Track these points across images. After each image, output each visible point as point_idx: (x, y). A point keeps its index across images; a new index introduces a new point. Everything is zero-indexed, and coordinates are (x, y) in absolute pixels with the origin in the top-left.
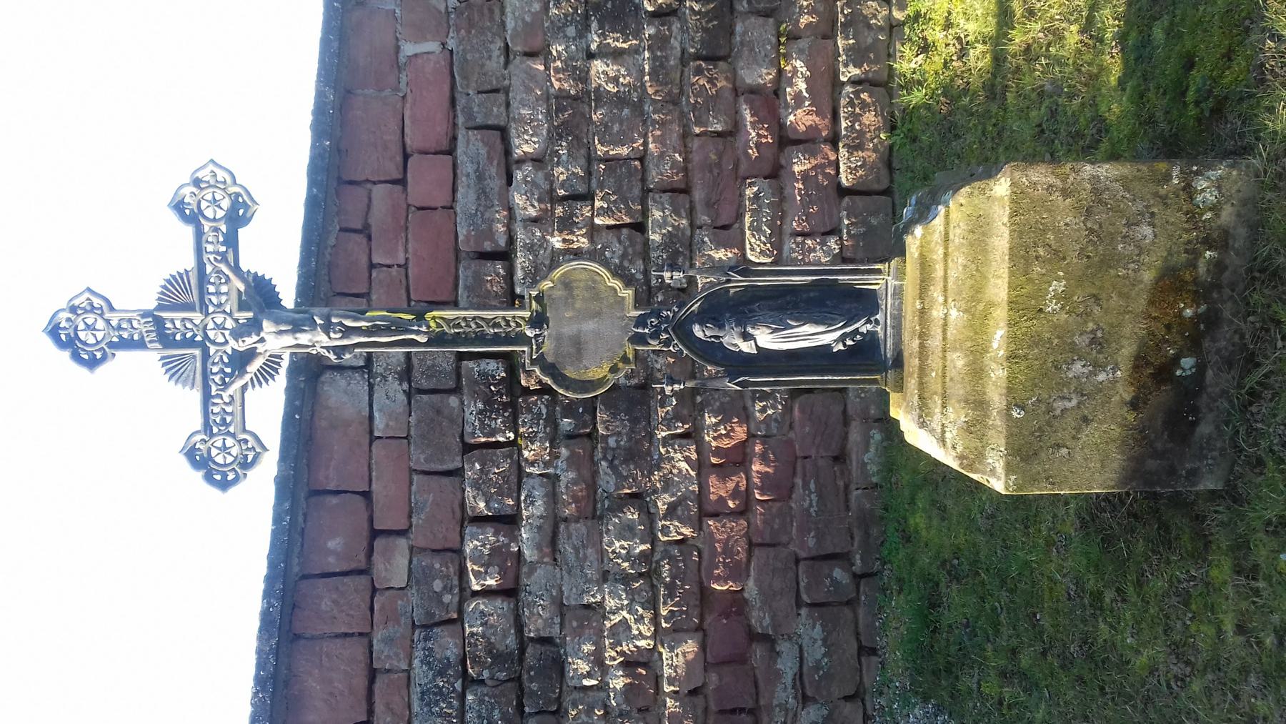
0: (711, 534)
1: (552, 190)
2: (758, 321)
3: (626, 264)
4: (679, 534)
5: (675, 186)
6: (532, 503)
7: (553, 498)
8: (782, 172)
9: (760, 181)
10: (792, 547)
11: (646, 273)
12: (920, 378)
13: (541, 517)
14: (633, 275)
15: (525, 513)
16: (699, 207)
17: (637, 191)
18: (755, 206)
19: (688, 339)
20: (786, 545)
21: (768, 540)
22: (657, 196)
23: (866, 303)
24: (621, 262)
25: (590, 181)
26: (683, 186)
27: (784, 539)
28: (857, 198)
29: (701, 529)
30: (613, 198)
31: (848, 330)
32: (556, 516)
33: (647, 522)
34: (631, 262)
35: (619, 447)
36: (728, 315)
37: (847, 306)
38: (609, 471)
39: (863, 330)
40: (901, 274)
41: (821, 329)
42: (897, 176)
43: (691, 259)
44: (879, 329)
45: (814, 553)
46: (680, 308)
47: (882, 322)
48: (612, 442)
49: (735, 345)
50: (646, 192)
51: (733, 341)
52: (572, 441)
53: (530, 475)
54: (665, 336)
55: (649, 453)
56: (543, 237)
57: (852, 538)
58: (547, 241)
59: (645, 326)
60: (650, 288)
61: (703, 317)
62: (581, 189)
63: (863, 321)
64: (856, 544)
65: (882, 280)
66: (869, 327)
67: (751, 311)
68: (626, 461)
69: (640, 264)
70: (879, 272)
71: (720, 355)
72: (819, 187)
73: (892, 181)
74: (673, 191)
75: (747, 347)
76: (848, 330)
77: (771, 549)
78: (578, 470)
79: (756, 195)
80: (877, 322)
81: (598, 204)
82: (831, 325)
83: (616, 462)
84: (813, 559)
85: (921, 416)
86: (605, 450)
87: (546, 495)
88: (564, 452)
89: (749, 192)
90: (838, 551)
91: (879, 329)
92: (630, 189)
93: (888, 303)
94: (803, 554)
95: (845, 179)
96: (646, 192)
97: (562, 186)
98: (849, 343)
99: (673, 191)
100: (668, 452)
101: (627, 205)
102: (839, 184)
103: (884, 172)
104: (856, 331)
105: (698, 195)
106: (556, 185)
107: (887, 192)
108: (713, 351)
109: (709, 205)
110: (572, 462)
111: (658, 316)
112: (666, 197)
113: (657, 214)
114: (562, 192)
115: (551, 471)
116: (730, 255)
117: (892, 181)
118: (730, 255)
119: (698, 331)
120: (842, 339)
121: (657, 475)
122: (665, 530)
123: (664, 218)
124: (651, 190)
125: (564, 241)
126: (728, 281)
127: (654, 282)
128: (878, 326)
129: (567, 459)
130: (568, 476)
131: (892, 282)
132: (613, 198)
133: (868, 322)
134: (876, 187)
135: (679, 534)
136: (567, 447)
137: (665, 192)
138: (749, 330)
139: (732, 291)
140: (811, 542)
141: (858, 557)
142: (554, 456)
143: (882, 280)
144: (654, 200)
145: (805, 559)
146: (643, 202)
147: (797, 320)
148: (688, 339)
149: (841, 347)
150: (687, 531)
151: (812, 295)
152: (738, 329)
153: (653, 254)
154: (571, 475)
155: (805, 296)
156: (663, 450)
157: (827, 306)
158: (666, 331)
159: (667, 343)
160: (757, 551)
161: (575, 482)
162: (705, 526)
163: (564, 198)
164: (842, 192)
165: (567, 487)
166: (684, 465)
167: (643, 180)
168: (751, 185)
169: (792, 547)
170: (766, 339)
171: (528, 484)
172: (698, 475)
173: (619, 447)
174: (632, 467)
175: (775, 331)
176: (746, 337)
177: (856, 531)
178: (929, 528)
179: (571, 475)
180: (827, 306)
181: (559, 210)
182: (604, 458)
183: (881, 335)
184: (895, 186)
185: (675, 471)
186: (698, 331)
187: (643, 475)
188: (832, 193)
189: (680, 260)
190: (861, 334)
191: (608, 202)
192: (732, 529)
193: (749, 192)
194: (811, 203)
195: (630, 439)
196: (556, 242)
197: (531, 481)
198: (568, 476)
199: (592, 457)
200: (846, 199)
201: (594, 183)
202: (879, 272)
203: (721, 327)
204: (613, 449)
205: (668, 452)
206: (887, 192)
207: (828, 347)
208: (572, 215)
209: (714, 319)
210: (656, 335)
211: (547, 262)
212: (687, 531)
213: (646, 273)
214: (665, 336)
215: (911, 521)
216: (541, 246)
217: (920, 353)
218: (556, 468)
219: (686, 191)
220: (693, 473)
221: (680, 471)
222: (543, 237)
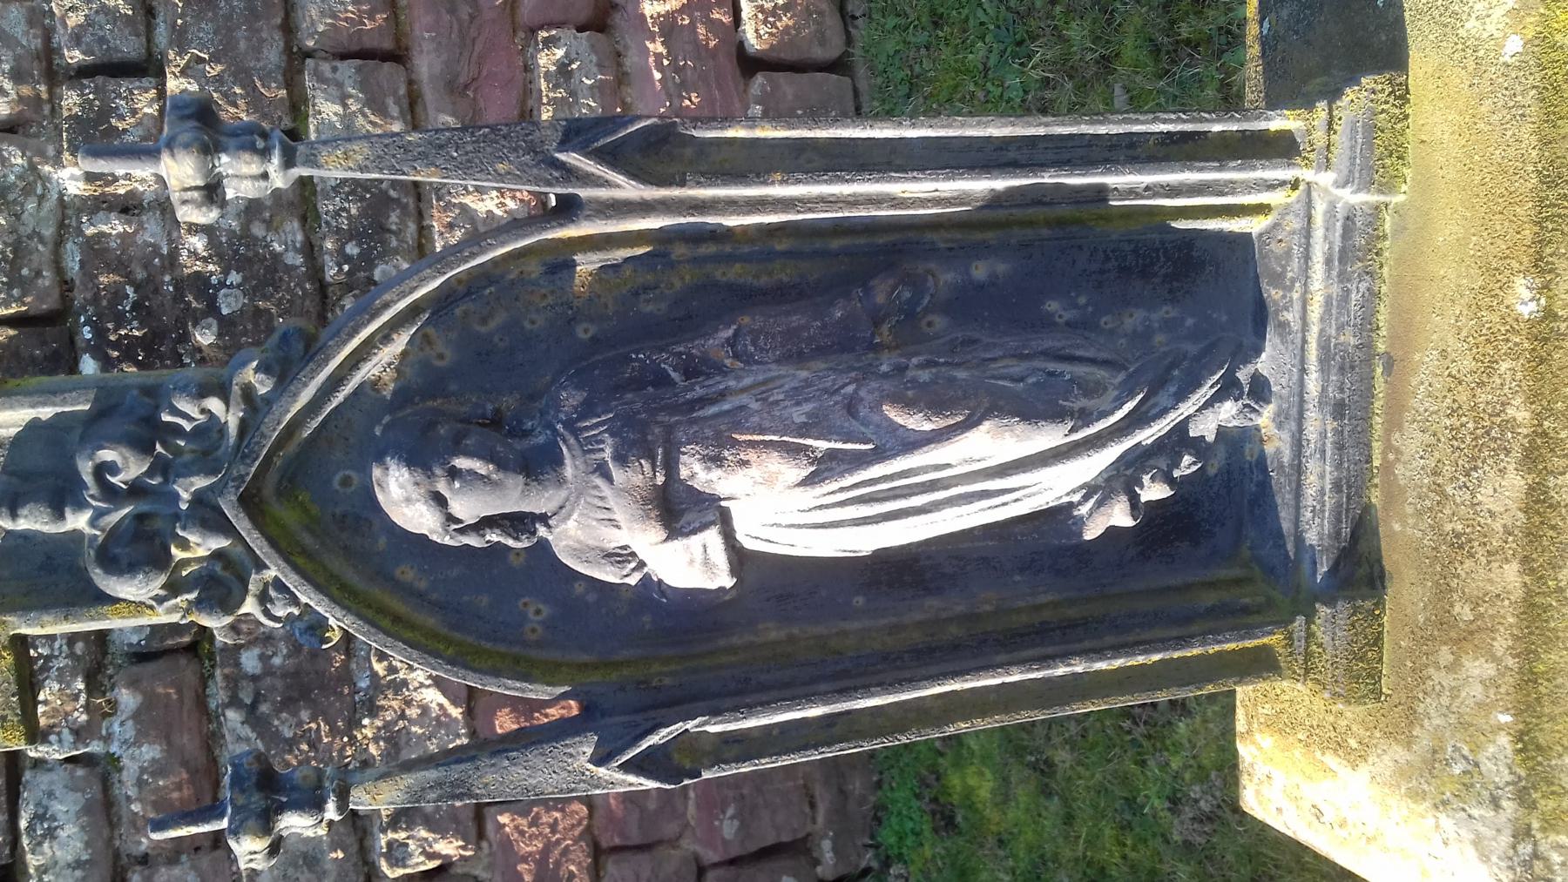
0: (507, 844)
1: (49, 53)
2: (737, 419)
3: (258, 230)
4: (432, 856)
5: (369, 43)
6: (51, 834)
7: (104, 810)
8: (617, 19)
9: (568, 34)
10: (688, 845)
11: (310, 250)
12: (1527, 652)
13: (78, 864)
14: (276, 257)
15: (33, 861)
16: (429, 94)
17: (273, 55)
18: (561, 93)
19: (348, 549)
20: (673, 843)
21: (635, 837)
22: (325, 67)
23: (1200, 297)
24: (246, 227)
25: (150, 29)
26: (387, 44)
27: (670, 829)
28: (781, 77)
29: (481, 835)
30: (214, 70)
31: (1146, 436)
32: (117, 855)
33: (351, 840)
34: (269, 224)
35: (268, 671)
36: (571, 399)
37: (1133, 319)
38: (246, 731)
39: (1205, 428)
40: (1379, 158)
41: (1051, 436)
42: (861, 31)
43: (420, 215)
44: (1265, 419)
45: (735, 852)
46: (285, 372)
47: (1279, 385)
48: (250, 661)
49: (623, 556)
50: (296, 57)
51: (604, 529)
52: (150, 667)
53: (38, 764)
54: (200, 546)
55: (345, 676)
56: (33, 167)
57: (813, 805)
58: (45, 179)
59: (63, 496)
60: (322, 287)
61: (427, 421)
62: (129, 47)
63: (1206, 391)
64: (820, 819)
65: (1291, 198)
66: (1228, 412)
67: (692, 371)
68: (289, 704)
69: (293, 231)
70: (1283, 148)
71: (536, 612)
72: (699, 50)
73: (849, 40)
74: (364, 54)
75: (690, 565)
76: (1146, 436)
77: (643, 860)
78: (167, 738)
79: (563, 69)
80: (1260, 390)
81: (173, 85)
82: (1085, 418)
83: (264, 708)
84: (732, 862)
85: (1522, 833)
86: (233, 682)
87: (87, 810)
88: (127, 699)
89: (547, 60)
90: (786, 838)
91: (1265, 419)
92: (257, 50)
93: (1309, 300)
94: (711, 856)
95: (755, 36)
96: (296, 57)
97: (76, 39)
98: (1154, 491)
99: (364, 54)
100: (392, 670)
101: (251, 90)
102: (741, 45)
103: (833, 22)
104: (1179, 439)
105: (426, 64)
106: (60, 38)
107: (839, 66)
108: (495, 607)
109: (455, 89)
110: (150, 721)
111: (146, 433)
112: (347, 69)
113: (327, 110)
114: (74, 56)
115: (95, 747)
116: (511, 205)
117: (849, 40)
118: (511, 205)
119: (402, 498)
120: (1122, 479)
121: (368, 727)
122: (397, 854)
123: (347, 118)
124: (309, 54)
125: (90, 177)
126: (568, 209)
127: (331, 272)
128: (1278, 410)
129: (136, 716)
130: (138, 756)
131: (1330, 189)
132: (214, 70)
133: (1229, 388)
134: (819, 53)
135: (432, 856)
136: (133, 684)
137: (344, 56)
138: (695, 471)
139: (587, 264)
140: (729, 829)
141: (827, 845)
142: (101, 714)
143: (1291, 198)
144: (321, 79)
145: (715, 865)
146: (291, 78)
147: (934, 404)
148: (348, 549)
149: (1120, 516)
150: (449, 847)
151: (980, 271)
152: (637, 476)
153: (326, 207)
154: (150, 752)
155: (946, 277)
156: (379, 668)
157: (1046, 324)
158: (207, 515)
159: (221, 584)
160: (611, 868)
161: (158, 769)
162: (490, 827)
163: (84, 72)
164: (750, 64)
165: (140, 783)
166: (433, 697)
167: (288, 29)
168: (549, 43)
169: (688, 845)
170: (779, 506)
171: (34, 788)
172: (469, 713)
173: (268, 671)
174: (305, 715)
175: (825, 468)
176: (678, 510)
177: (818, 790)
178: (1004, 797)
179: (150, 752)
180: (1046, 324)
181: (71, 100)
182: (234, 702)
183: (1277, 444)
184: (857, 52)
185: (413, 712)
186: (402, 498)
187: (334, 731)
188: (730, 67)
189: (394, 217)
190: (1198, 447)
191: (201, 78)
192: (553, 827)
193: (547, 60)
194: (684, 85)
195: (296, 649)
196: (70, 178)
197: (43, 780)
198: (138, 756)
199: (201, 701)
200: (760, 79)
201: (162, 34)
202: (1283, 148)
203: (537, 465)
204: (254, 678)
205: (392, 670)
206: (839, 66)
207: (1058, 517)
208: (106, 112)
209: (495, 422)
210: (139, 547)
211: (48, 232)
212: (449, 847)
213: (310, 250)
214: (200, 546)
215: (955, 781)
216: (28, 191)
217: (1532, 535)
218: (108, 739)
219: (398, 56)
220: (456, 712)
221: (425, 709)
222: (33, 167)
